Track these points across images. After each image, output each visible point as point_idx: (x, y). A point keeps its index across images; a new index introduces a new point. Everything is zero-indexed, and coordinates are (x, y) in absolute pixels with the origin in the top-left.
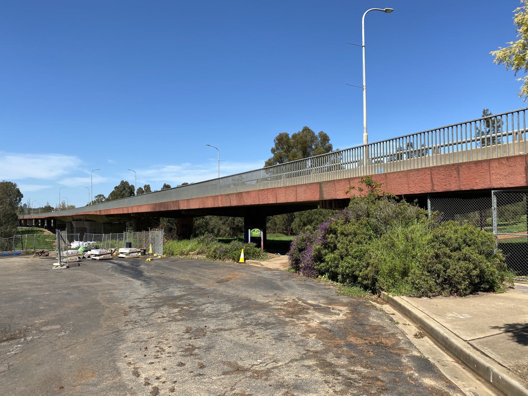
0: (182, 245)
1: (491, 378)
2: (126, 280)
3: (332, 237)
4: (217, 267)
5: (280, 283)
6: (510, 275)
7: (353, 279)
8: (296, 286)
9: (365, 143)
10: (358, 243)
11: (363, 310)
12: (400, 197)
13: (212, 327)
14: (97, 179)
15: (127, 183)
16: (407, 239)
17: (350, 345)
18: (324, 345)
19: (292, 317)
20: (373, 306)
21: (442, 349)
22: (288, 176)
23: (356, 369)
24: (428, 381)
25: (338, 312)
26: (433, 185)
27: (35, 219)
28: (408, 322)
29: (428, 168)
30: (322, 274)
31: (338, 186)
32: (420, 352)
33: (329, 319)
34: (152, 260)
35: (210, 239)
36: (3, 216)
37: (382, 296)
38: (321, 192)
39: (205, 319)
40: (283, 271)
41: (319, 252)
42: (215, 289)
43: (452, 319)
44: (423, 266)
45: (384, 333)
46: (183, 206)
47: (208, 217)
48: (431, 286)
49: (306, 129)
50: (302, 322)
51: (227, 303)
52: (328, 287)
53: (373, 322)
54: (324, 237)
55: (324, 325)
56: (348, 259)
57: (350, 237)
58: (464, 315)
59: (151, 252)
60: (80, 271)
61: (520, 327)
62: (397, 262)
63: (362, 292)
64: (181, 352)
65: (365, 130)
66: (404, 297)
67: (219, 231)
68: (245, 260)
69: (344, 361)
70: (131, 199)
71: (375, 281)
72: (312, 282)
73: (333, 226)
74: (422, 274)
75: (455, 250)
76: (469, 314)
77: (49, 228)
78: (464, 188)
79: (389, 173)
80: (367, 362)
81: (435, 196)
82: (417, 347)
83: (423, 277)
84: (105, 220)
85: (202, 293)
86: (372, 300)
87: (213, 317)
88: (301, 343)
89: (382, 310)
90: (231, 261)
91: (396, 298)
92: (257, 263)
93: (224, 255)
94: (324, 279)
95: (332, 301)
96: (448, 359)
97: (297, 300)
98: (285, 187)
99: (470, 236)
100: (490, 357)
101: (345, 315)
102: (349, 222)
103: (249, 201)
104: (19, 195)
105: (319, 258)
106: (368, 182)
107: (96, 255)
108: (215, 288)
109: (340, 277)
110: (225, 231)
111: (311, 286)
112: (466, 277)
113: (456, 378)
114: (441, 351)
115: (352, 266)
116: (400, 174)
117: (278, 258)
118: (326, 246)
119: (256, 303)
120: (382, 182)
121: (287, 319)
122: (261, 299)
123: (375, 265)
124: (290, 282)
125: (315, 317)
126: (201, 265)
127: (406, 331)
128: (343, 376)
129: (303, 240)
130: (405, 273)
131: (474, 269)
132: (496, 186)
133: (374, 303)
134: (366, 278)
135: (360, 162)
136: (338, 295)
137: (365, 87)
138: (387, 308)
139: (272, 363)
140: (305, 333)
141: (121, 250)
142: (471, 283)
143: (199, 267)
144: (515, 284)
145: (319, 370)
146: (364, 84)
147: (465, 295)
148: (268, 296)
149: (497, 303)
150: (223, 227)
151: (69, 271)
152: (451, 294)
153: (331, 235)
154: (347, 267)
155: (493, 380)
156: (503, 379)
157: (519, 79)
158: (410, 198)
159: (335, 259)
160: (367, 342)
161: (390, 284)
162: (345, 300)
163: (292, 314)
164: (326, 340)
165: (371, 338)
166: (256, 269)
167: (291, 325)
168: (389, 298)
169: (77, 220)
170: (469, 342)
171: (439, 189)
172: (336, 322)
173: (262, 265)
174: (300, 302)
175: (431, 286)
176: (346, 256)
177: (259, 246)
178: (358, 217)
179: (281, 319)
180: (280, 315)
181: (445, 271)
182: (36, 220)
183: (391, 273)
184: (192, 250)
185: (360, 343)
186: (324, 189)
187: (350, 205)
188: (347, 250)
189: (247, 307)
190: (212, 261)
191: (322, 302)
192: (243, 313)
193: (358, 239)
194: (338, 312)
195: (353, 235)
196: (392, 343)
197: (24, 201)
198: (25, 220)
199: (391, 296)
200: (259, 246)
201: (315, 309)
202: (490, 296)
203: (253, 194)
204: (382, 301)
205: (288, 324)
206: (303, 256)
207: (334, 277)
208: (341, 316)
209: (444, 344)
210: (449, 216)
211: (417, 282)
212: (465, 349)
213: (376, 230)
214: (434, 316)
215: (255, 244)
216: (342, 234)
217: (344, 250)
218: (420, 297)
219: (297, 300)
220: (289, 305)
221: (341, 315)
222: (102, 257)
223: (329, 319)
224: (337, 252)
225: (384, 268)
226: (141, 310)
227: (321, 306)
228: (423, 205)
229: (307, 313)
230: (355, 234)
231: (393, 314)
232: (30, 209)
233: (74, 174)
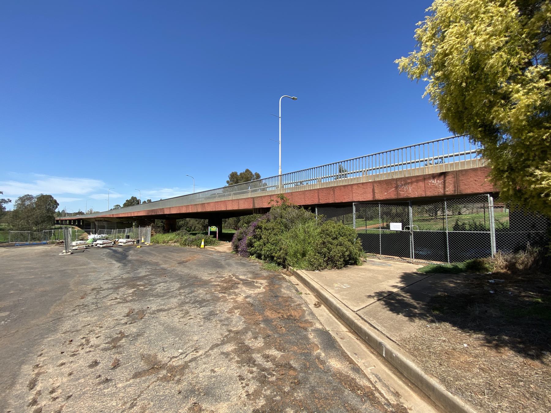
0: (165, 237)
1: (384, 352)
2: (110, 263)
3: (259, 231)
4: (184, 251)
5: (223, 263)
6: (363, 253)
7: (271, 258)
8: (234, 264)
9: (280, 174)
10: (275, 234)
11: (277, 282)
12: (300, 206)
13: (154, 307)
14: (115, 196)
15: (135, 198)
16: (305, 232)
17: (267, 321)
18: (245, 322)
19: (224, 293)
20: (284, 279)
21: (336, 318)
22: (235, 194)
23: (270, 353)
24: (335, 364)
25: (259, 285)
26: (319, 199)
27: (69, 220)
28: (308, 292)
29: (317, 189)
30: (252, 255)
31: (264, 200)
32: (321, 323)
33: (252, 292)
34: (141, 247)
35: (184, 233)
36: (40, 217)
37: (289, 270)
38: (254, 203)
39: (152, 299)
40: (228, 253)
41: (251, 241)
42: (174, 269)
43: (338, 290)
44: (315, 249)
45: (293, 305)
46: (167, 212)
47: (188, 219)
48: (320, 263)
49: (247, 171)
50: (232, 297)
51: (177, 282)
52: (255, 264)
53: (284, 294)
54: (254, 231)
55: (248, 300)
56: (269, 245)
57: (270, 231)
58: (345, 285)
59: (143, 241)
60: (79, 257)
61: (385, 295)
62: (299, 247)
63: (277, 267)
64: (106, 343)
65: (280, 168)
66: (304, 271)
67: (195, 228)
68: (205, 246)
69: (259, 343)
70: (138, 206)
71: (285, 260)
72: (245, 260)
73: (260, 224)
74: (315, 255)
75: (334, 239)
76: (347, 283)
77: (79, 226)
78: (337, 201)
79: (294, 192)
80: (280, 341)
81: (320, 206)
82: (318, 318)
83: (315, 257)
84: (118, 220)
85: (163, 272)
86: (283, 273)
87: (160, 297)
88: (225, 322)
89: (290, 282)
90: (195, 247)
91: (299, 272)
92: (212, 248)
93: (192, 243)
94: (253, 257)
95: (256, 276)
96: (343, 329)
97: (232, 276)
98: (232, 200)
99: (343, 231)
100: (378, 330)
101: (264, 288)
102: (270, 221)
103: (209, 209)
104: (56, 204)
105: (251, 245)
106: (282, 197)
107: (100, 244)
108: (175, 268)
109: (263, 257)
110: (199, 228)
111: (244, 263)
112: (342, 256)
113: (356, 354)
114: (337, 321)
115: (271, 250)
116: (300, 193)
117: (227, 244)
118: (255, 237)
119: (201, 280)
120: (290, 197)
121: (220, 295)
122: (205, 277)
123: (285, 249)
124: (231, 261)
125: (242, 291)
126: (175, 250)
127: (308, 301)
128: (259, 366)
129: (241, 233)
130: (304, 255)
131: (346, 251)
132: (355, 200)
133: (284, 276)
134: (279, 258)
135: (277, 187)
136: (261, 270)
137: (280, 142)
138: (293, 279)
139: (192, 353)
140: (232, 309)
141: (121, 240)
142: (344, 261)
143: (172, 251)
144: (367, 259)
145: (237, 359)
146: (280, 140)
147: (341, 268)
148: (211, 274)
149: (361, 274)
150: (198, 225)
151: (71, 256)
152: (332, 268)
153: (258, 230)
154: (267, 251)
155: (385, 354)
156: (397, 358)
157: (425, 79)
158: (306, 207)
159: (260, 245)
160: (280, 315)
161: (295, 262)
162: (265, 274)
163: (225, 289)
164: (248, 317)
165: (283, 310)
166: (211, 252)
167: (222, 301)
168: (294, 271)
169: (98, 221)
170: (357, 312)
171: (322, 202)
172: (258, 295)
173: (215, 249)
174: (234, 278)
175: (320, 263)
176: (267, 243)
177: (215, 237)
178: (275, 218)
179: (216, 295)
180: (216, 291)
181: (329, 253)
182: (70, 221)
183: (295, 255)
184: (171, 240)
185: (275, 317)
186: (256, 201)
187: (271, 211)
188: (268, 239)
189: (192, 285)
190: (183, 247)
191: (249, 277)
192: (187, 290)
193: (275, 231)
194: (259, 285)
195: (272, 230)
196: (299, 315)
197: (59, 209)
198: (62, 221)
199: (295, 270)
200: (215, 237)
201: (244, 284)
202: (355, 268)
203: (212, 204)
204: (289, 274)
205: (220, 300)
206: (241, 244)
207: (259, 257)
208: (262, 290)
209: (337, 312)
210: (329, 217)
211: (312, 260)
212: (356, 321)
213: (286, 226)
214: (325, 287)
215: (212, 236)
216: (265, 229)
217: (266, 239)
218: (314, 270)
219: (232, 276)
220: (225, 281)
221: (262, 288)
222: (105, 245)
223: (252, 292)
224: (261, 240)
225: (291, 251)
226: (101, 292)
227: (248, 280)
228: (313, 211)
229: (237, 288)
230: (273, 229)
231: (298, 285)
232: (65, 214)
233: (100, 191)
